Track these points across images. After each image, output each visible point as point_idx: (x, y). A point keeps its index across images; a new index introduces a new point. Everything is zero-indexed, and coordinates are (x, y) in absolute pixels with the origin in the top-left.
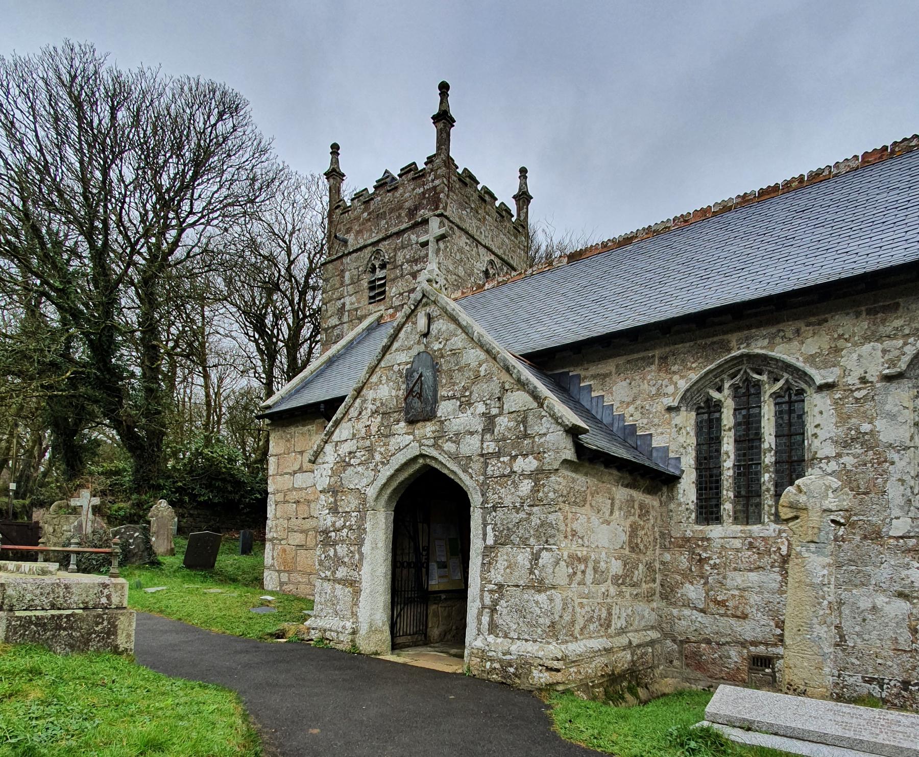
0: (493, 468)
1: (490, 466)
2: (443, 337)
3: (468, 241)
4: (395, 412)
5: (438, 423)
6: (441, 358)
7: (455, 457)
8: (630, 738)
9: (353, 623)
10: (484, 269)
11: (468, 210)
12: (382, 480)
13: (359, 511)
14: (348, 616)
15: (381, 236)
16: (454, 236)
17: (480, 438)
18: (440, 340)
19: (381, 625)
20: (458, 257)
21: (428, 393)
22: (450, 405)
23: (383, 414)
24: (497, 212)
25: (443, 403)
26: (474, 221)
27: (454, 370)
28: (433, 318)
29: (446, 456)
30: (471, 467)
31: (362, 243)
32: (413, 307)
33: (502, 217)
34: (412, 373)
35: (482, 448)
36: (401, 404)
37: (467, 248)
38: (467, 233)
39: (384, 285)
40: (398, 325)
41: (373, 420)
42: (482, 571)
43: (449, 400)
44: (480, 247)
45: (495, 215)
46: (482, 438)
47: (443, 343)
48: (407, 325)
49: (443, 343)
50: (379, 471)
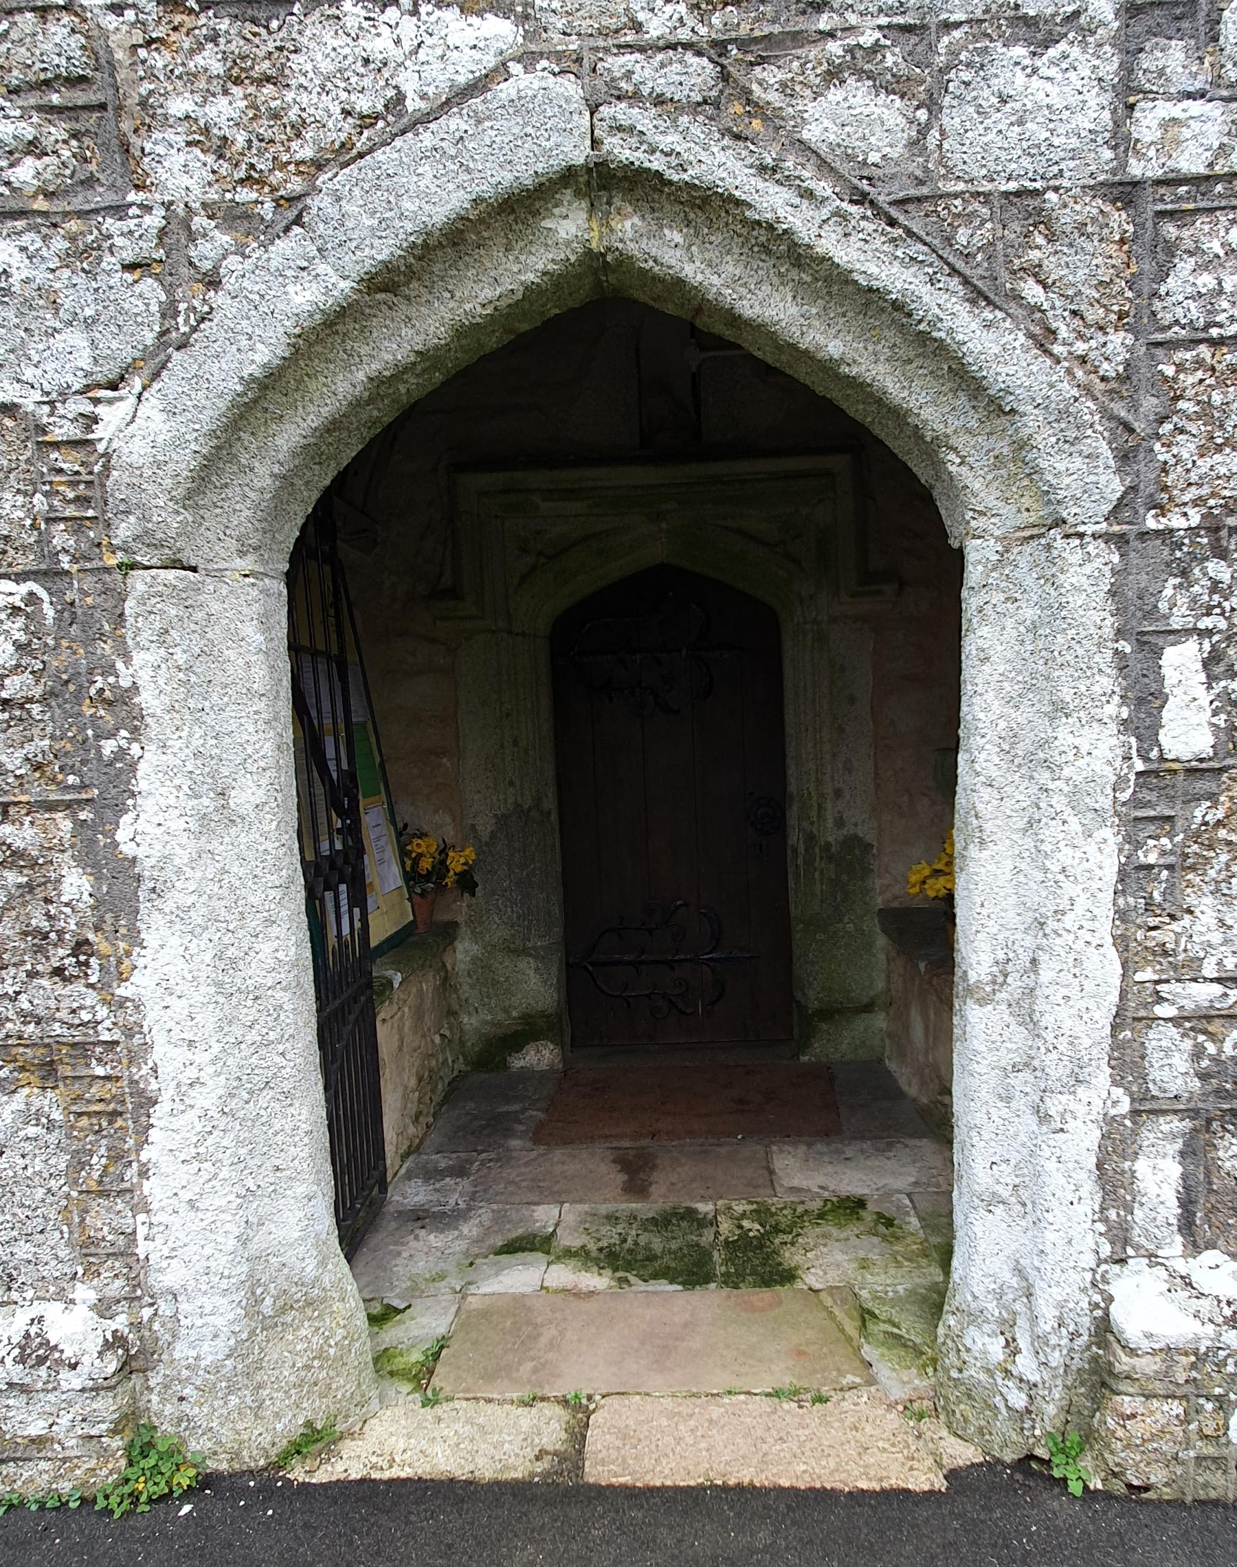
0: (1206, 281)
1: (1185, 265)
8: (226, 1029)
9: (104, 1308)
13: (50, 575)
14: (51, 1270)
17: (1110, 68)
19: (311, 1267)
29: (824, 188)
30: (1036, 272)
35: (1122, 142)
42: (1122, 915)
46: (1127, 69)
50: (212, 281)
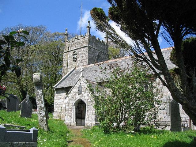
7: (84, 99)
12: (75, 102)
15: (76, 49)
21: (81, 91)
31: (72, 49)
39: (76, 58)
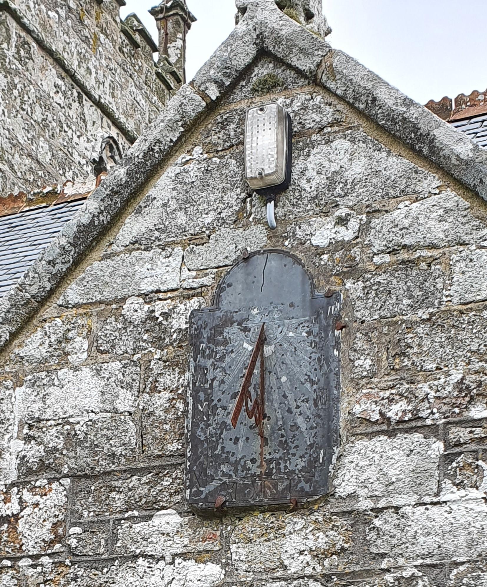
2: (351, 200)
3: (60, 82)
4: (133, 472)
5: (339, 522)
6: (343, 276)
10: (96, 156)
11: (63, 13)
16: (30, 64)
18: (342, 212)
20: (38, 115)
22: (399, 455)
23: (74, 476)
24: (125, 32)
25: (361, 444)
26: (75, 40)
27: (411, 326)
28: (304, 133)
32: (213, 93)
33: (136, 45)
34: (218, 330)
36: (161, 441)
37: (59, 98)
38: (59, 62)
40: (149, 153)
41: (27, 496)
43: (391, 433)
44: (87, 103)
45: (120, 38)
47: (354, 224)
48: (182, 157)
49: (354, 224)
